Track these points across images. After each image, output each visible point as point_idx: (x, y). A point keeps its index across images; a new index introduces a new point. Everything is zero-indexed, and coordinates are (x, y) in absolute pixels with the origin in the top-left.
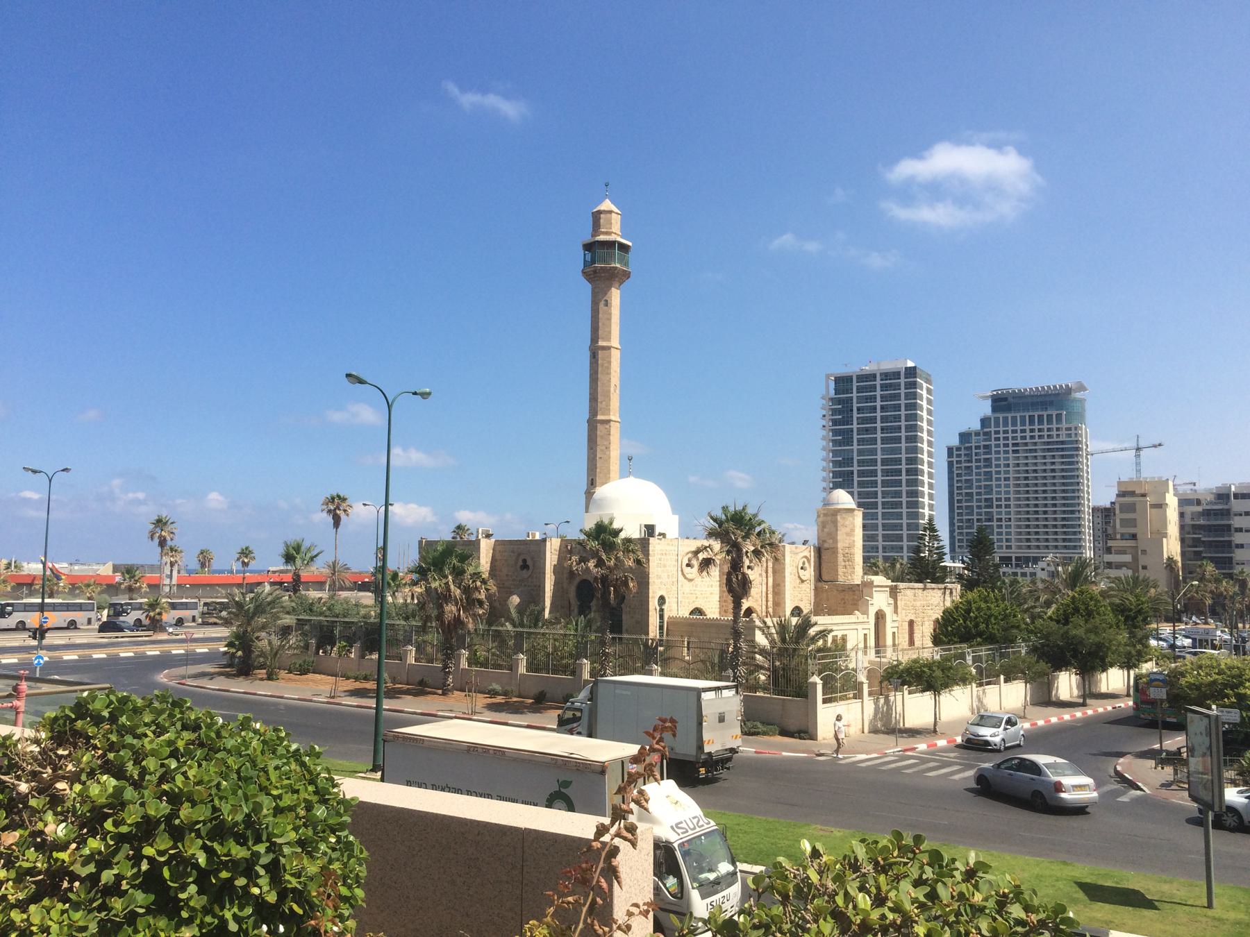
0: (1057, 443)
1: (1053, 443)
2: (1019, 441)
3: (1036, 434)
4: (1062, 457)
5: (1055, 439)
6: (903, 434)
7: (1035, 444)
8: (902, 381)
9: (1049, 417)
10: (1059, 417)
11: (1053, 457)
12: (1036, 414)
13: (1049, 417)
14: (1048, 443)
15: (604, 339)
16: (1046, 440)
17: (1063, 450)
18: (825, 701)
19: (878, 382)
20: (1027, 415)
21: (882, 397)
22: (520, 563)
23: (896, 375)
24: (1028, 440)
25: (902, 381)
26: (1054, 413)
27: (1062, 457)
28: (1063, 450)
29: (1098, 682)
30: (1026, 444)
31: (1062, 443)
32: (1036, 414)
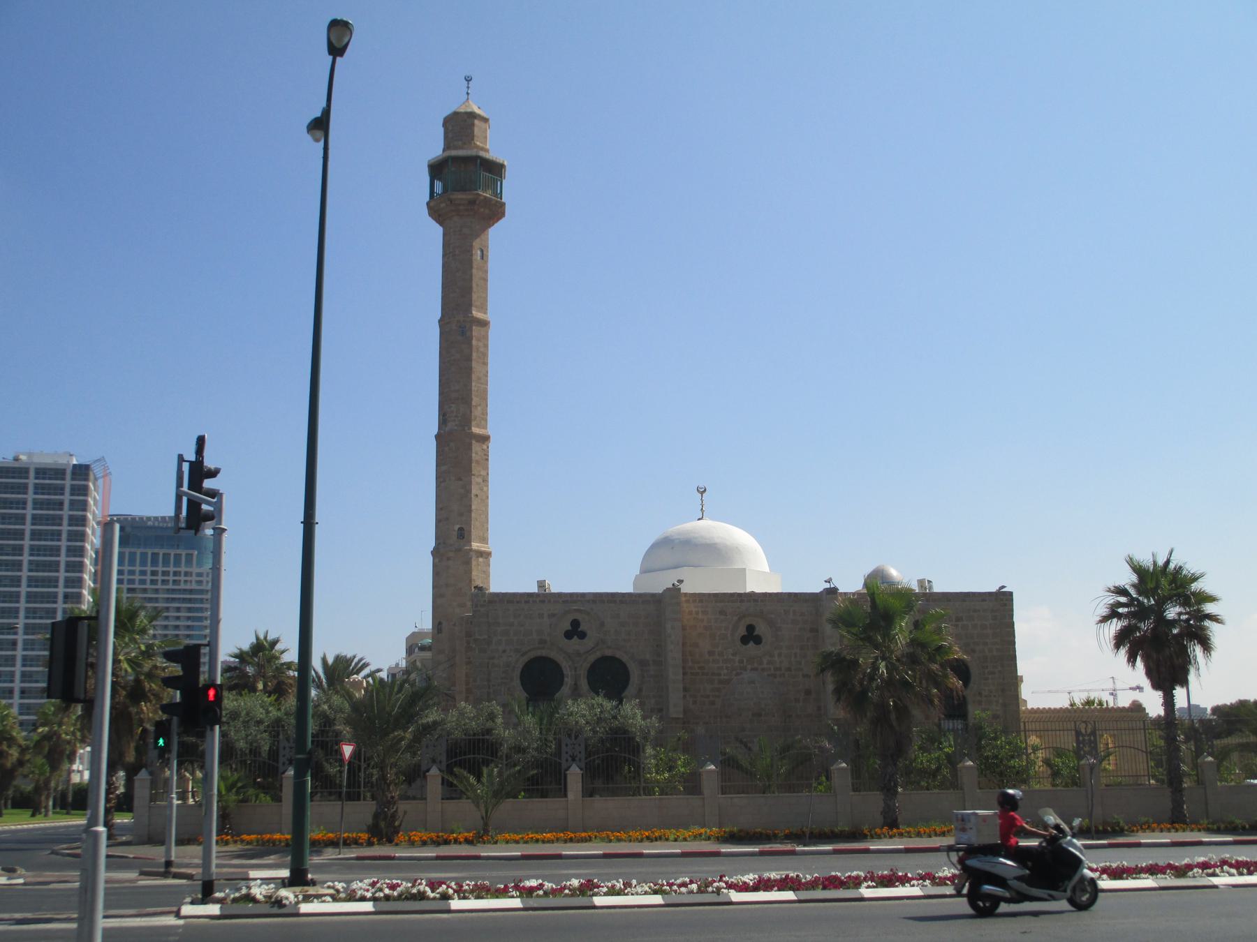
0: (185, 591)
1: (180, 591)
2: (136, 586)
3: (149, 577)
4: (190, 610)
5: (182, 586)
6: (63, 559)
7: (157, 591)
8: (68, 483)
9: (178, 557)
10: (189, 556)
11: (178, 609)
12: (162, 552)
13: (166, 556)
14: (173, 591)
15: (478, 426)
16: (170, 586)
17: (190, 601)
18: (105, 917)
19: (32, 481)
20: (150, 552)
21: (35, 502)
22: (742, 631)
23: (59, 473)
24: (148, 586)
25: (68, 483)
26: (184, 553)
27: (190, 610)
28: (190, 601)
29: (1181, 720)
30: (145, 590)
31: (191, 591)
32: (162, 552)
